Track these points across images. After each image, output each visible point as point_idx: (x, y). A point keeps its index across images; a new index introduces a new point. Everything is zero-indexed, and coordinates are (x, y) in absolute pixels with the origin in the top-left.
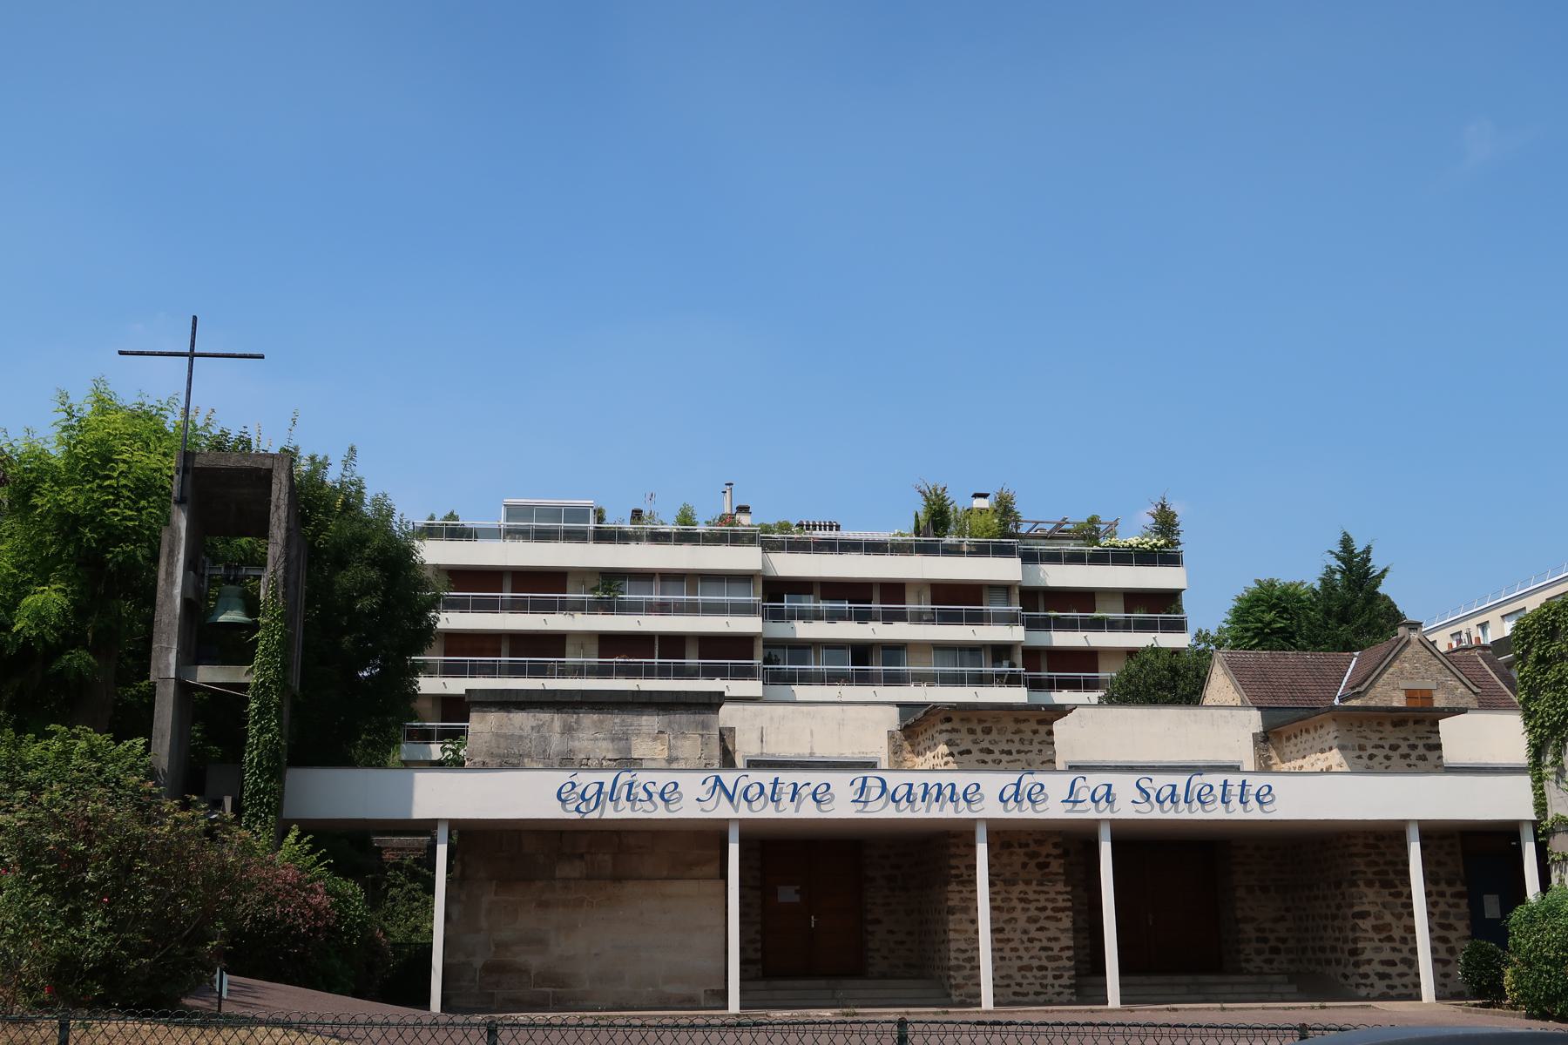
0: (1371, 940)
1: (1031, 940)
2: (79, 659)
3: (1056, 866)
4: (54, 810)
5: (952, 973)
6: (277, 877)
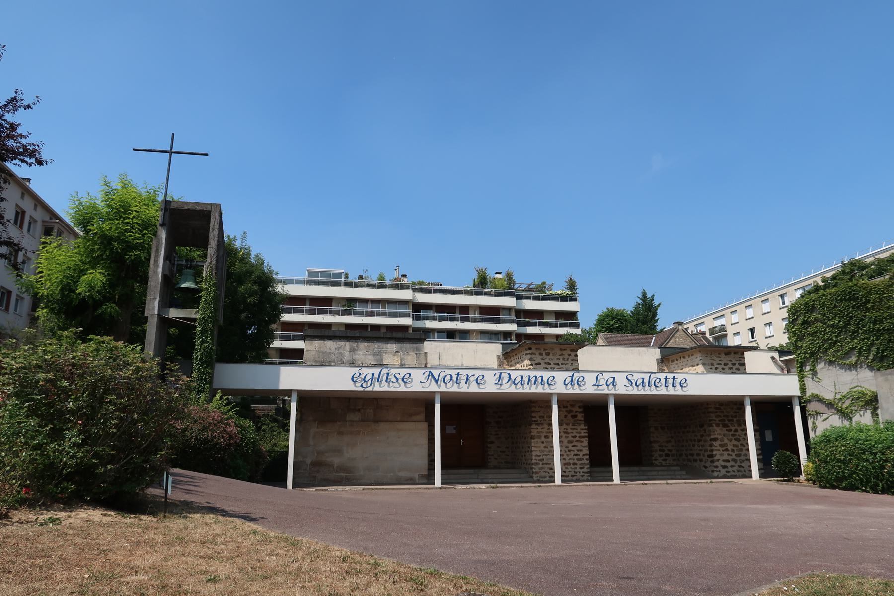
0: (719, 450)
1: (569, 451)
2: (110, 308)
3: (580, 417)
4: (46, 357)
5: (534, 466)
6: (209, 416)
